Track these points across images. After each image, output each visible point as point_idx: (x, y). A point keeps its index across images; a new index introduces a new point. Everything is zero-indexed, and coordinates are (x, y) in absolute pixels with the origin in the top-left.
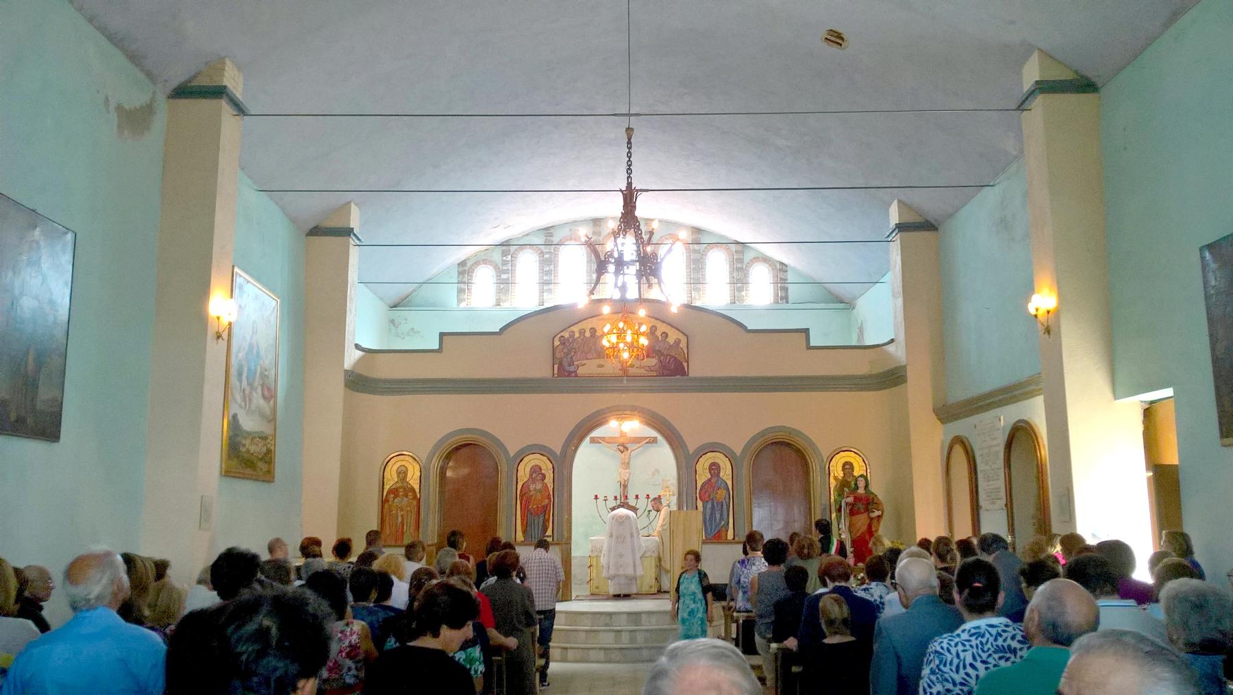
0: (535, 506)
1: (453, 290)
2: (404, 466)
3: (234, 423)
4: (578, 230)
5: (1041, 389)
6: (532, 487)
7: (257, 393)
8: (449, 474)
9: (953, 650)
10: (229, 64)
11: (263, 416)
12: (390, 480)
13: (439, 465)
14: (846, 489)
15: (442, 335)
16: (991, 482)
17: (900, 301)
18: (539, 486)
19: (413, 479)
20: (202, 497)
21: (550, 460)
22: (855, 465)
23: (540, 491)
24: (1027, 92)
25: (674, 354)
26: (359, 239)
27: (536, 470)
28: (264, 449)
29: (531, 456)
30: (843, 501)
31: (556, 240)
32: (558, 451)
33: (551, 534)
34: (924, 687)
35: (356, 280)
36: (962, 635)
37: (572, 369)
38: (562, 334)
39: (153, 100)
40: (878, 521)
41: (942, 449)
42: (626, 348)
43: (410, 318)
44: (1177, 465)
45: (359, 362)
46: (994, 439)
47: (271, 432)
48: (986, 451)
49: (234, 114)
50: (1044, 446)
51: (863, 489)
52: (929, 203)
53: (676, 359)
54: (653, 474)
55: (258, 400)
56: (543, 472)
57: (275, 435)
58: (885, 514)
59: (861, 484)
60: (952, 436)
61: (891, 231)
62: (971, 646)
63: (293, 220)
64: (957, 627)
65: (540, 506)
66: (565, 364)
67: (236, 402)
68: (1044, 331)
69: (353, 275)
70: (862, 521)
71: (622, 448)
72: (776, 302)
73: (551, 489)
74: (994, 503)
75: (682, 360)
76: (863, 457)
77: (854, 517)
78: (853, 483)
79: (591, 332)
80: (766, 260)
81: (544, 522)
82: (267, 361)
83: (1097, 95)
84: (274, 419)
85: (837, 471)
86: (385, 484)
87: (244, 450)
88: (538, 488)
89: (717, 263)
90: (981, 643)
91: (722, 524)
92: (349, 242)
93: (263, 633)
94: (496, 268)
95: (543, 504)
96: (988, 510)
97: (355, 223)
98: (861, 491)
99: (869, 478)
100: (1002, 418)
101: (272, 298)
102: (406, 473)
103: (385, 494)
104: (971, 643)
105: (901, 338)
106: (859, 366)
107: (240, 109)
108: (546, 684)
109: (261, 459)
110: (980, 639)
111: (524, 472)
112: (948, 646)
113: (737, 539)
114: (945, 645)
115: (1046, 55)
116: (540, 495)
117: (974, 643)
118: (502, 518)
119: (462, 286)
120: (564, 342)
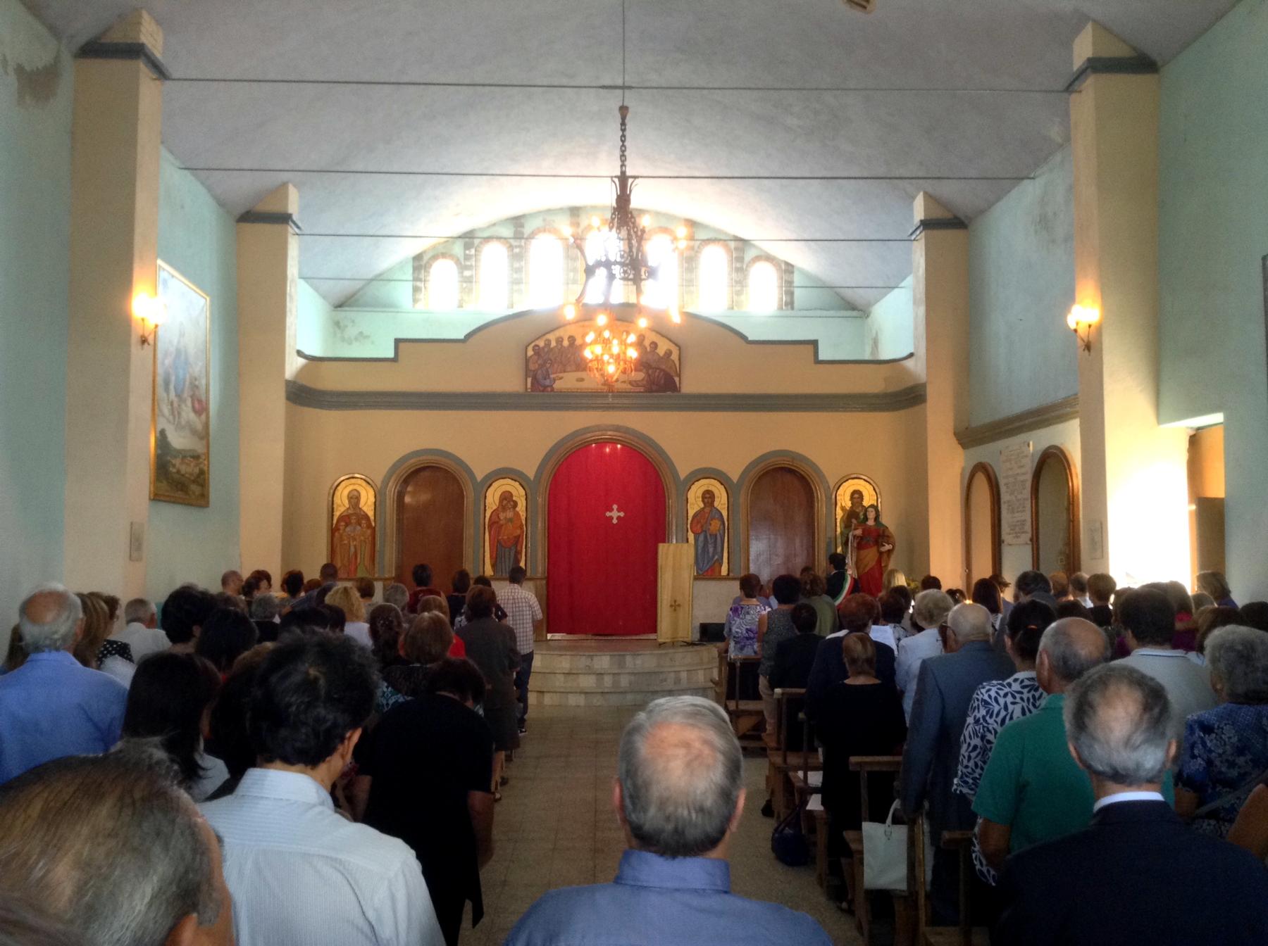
0: (505, 537)
1: (409, 287)
2: (356, 490)
3: (162, 440)
4: (554, 221)
5: (1077, 412)
6: (502, 516)
7: (186, 406)
8: (407, 499)
9: (1001, 701)
10: (146, 17)
11: (194, 432)
12: (340, 506)
13: (396, 490)
14: (854, 521)
15: (398, 342)
16: (1016, 515)
17: (922, 310)
18: (510, 514)
19: (367, 501)
20: (132, 523)
21: (522, 487)
22: (865, 494)
23: (510, 520)
24: (1078, 70)
25: (664, 367)
26: (298, 227)
27: (507, 498)
28: (197, 470)
30: (851, 534)
31: (527, 230)
35: (296, 275)
36: (1013, 684)
37: (547, 382)
38: (537, 343)
39: (57, 59)
40: (889, 556)
41: (962, 474)
42: (611, 360)
43: (363, 321)
44: (1221, 500)
45: (302, 370)
46: (1022, 467)
47: (205, 450)
48: (1011, 480)
49: (154, 77)
50: (1077, 474)
51: (873, 520)
52: (958, 194)
53: (664, 370)
55: (188, 414)
56: (514, 499)
57: (208, 453)
58: (896, 548)
59: (871, 515)
60: (975, 462)
61: (915, 228)
62: (1022, 699)
63: (221, 203)
64: (1009, 676)
65: (511, 537)
66: (540, 377)
67: (163, 416)
68: (1083, 347)
69: (293, 269)
70: (870, 555)
72: (780, 308)
73: (523, 518)
74: (1017, 537)
75: (673, 374)
76: (874, 485)
77: (862, 552)
78: (862, 514)
79: (569, 341)
80: (769, 258)
81: (515, 555)
82: (197, 368)
83: (1156, 76)
84: (207, 434)
85: (844, 500)
86: (335, 510)
87: (174, 470)
88: (508, 517)
89: (715, 259)
90: (1034, 696)
91: (715, 559)
92: (287, 230)
93: (309, 685)
94: (458, 262)
95: (515, 534)
96: (1010, 545)
97: (293, 207)
98: (871, 522)
99: (879, 508)
100: (1031, 443)
101: (200, 295)
102: (358, 498)
103: (335, 521)
104: (1022, 696)
105: (922, 352)
106: (874, 384)
107: (160, 72)
108: (524, 730)
109: (194, 482)
110: (1033, 692)
111: (493, 498)
112: (996, 695)
113: (731, 575)
114: (993, 694)
115: (1103, 28)
117: (1025, 696)
118: (468, 550)
119: (418, 284)
120: (537, 351)
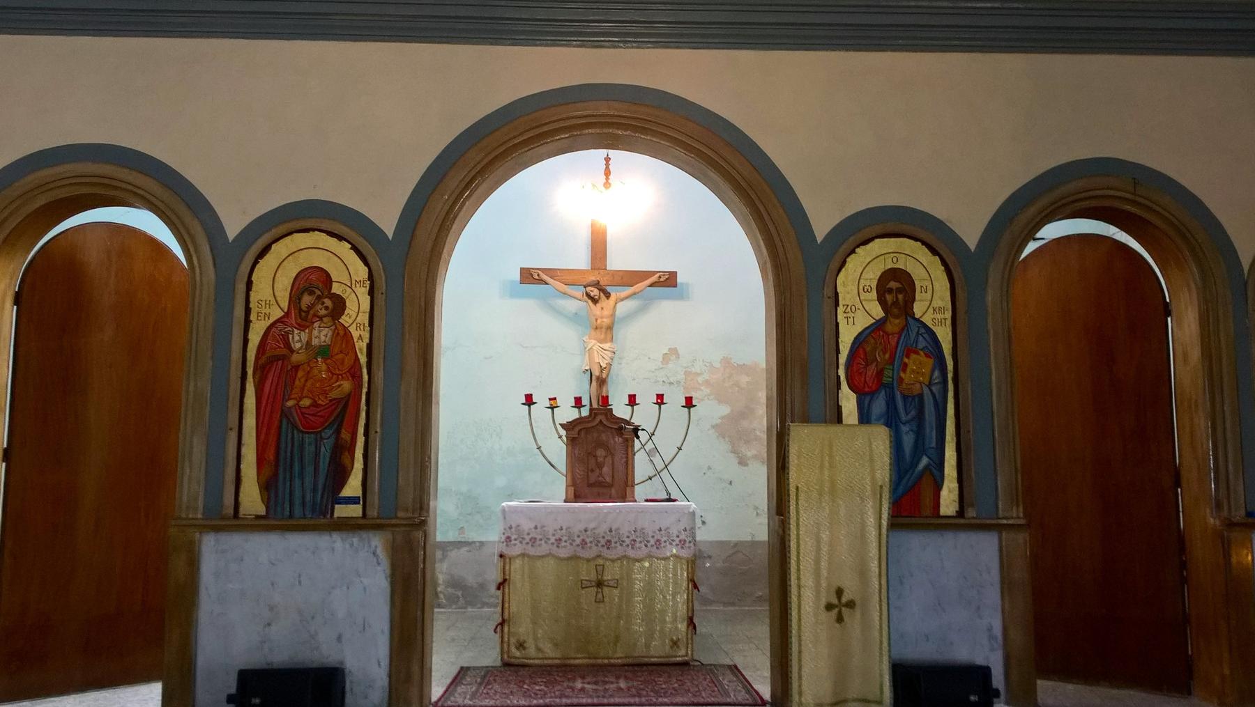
0: (306, 402)
6: (298, 339)
18: (322, 335)
23: (324, 352)
29: (300, 240)
32: (388, 223)
33: (359, 493)
34: (362, 353)
54: (666, 359)
56: (336, 289)
71: (595, 292)
95: (334, 394)
113: (971, 513)
116: (324, 367)
